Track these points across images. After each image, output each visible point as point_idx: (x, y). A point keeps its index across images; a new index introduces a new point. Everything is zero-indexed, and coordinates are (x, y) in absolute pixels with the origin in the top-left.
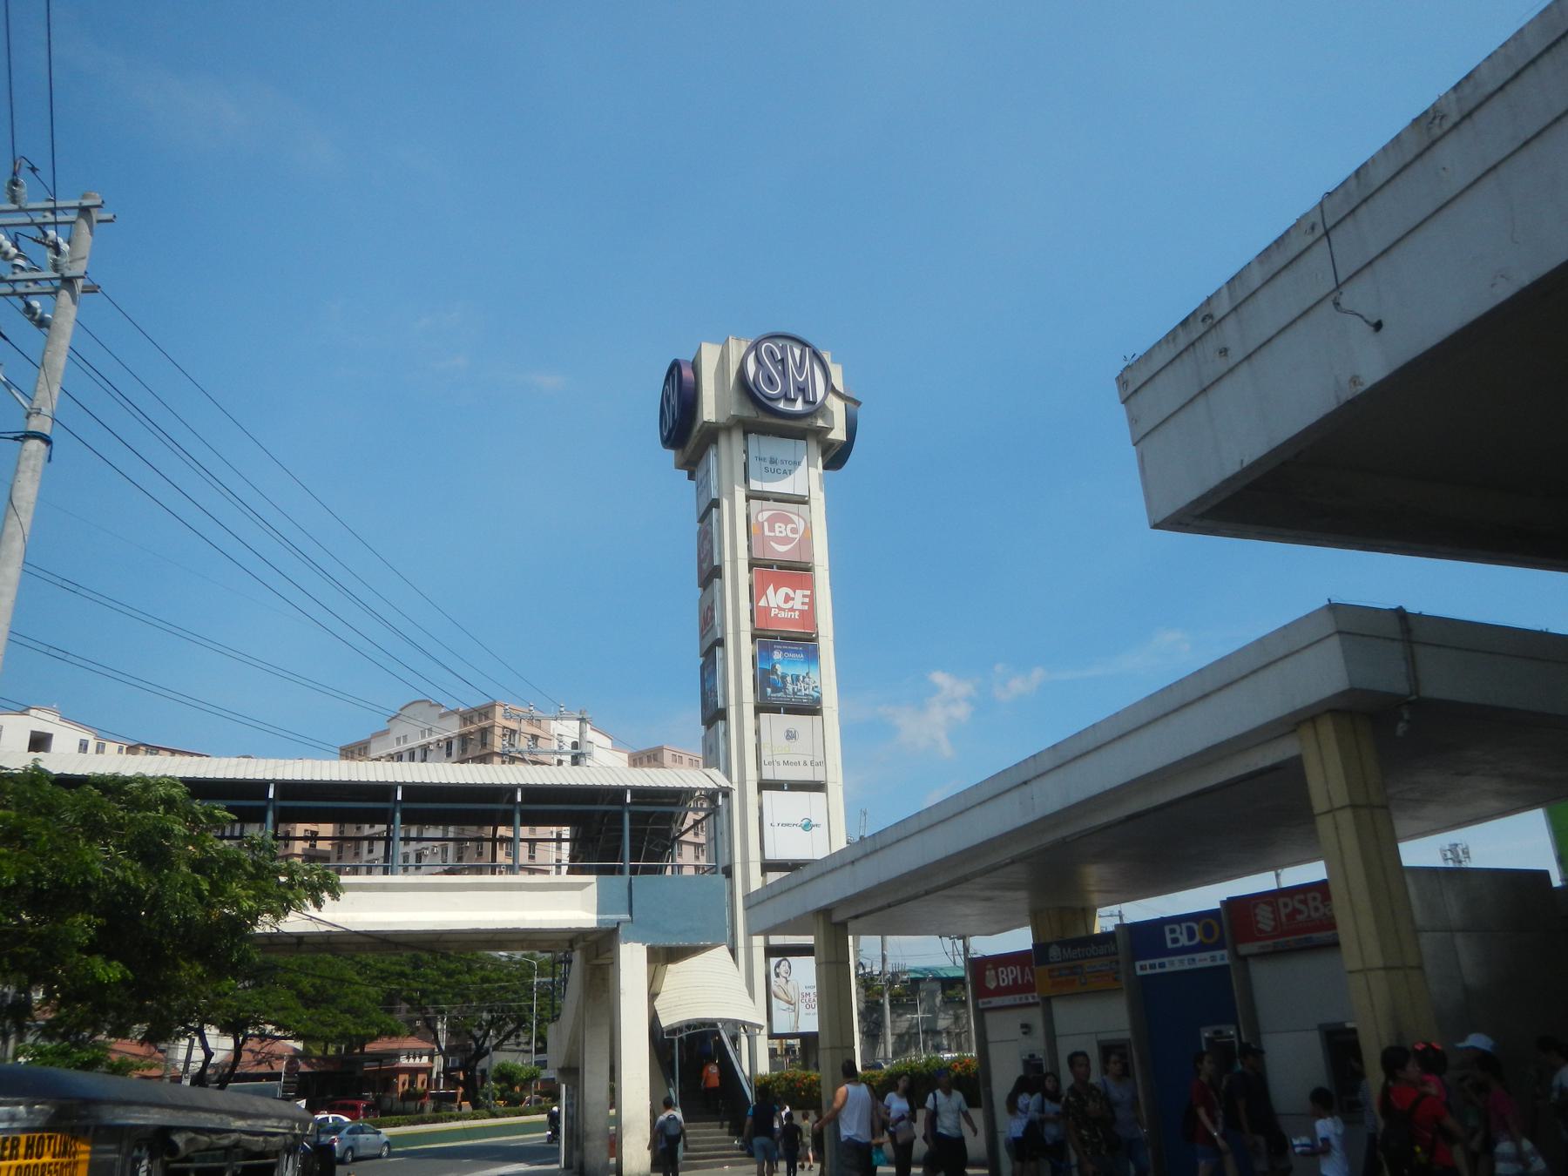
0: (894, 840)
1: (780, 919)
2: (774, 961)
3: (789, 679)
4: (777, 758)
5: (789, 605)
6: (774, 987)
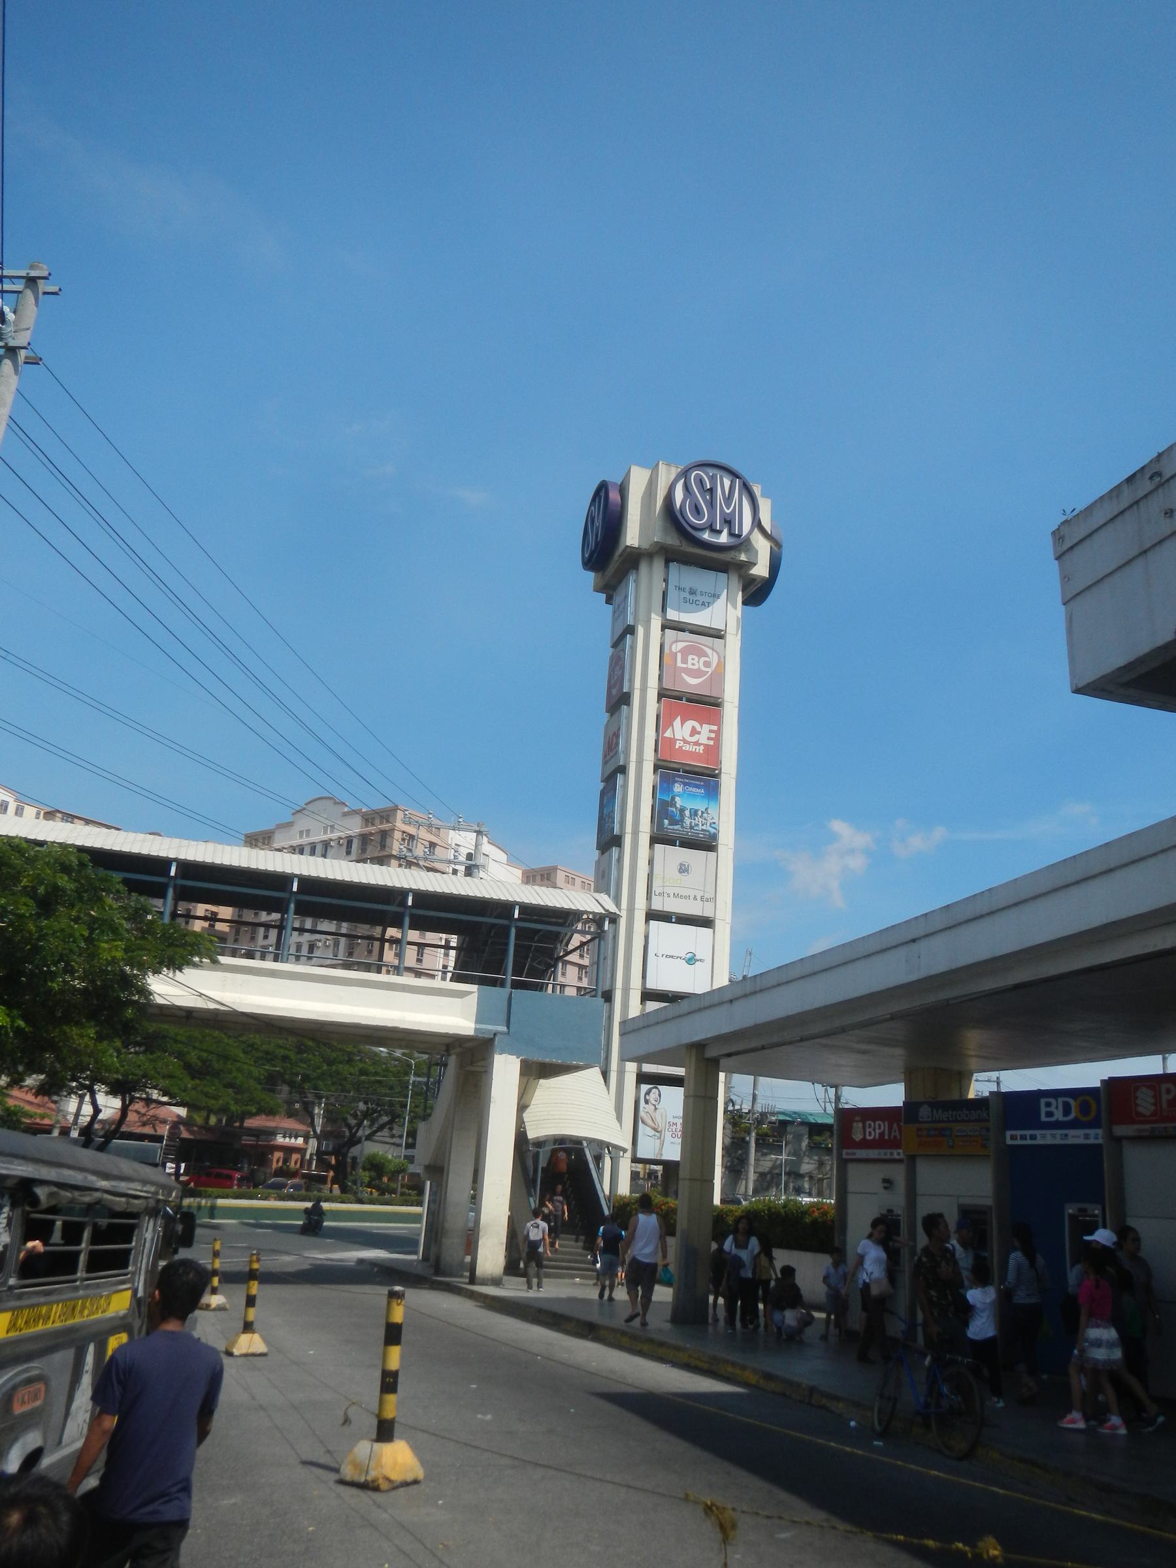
0: (775, 984)
1: (653, 1048)
2: (645, 1088)
3: (687, 813)
4: (667, 890)
5: (694, 739)
6: (642, 1113)
